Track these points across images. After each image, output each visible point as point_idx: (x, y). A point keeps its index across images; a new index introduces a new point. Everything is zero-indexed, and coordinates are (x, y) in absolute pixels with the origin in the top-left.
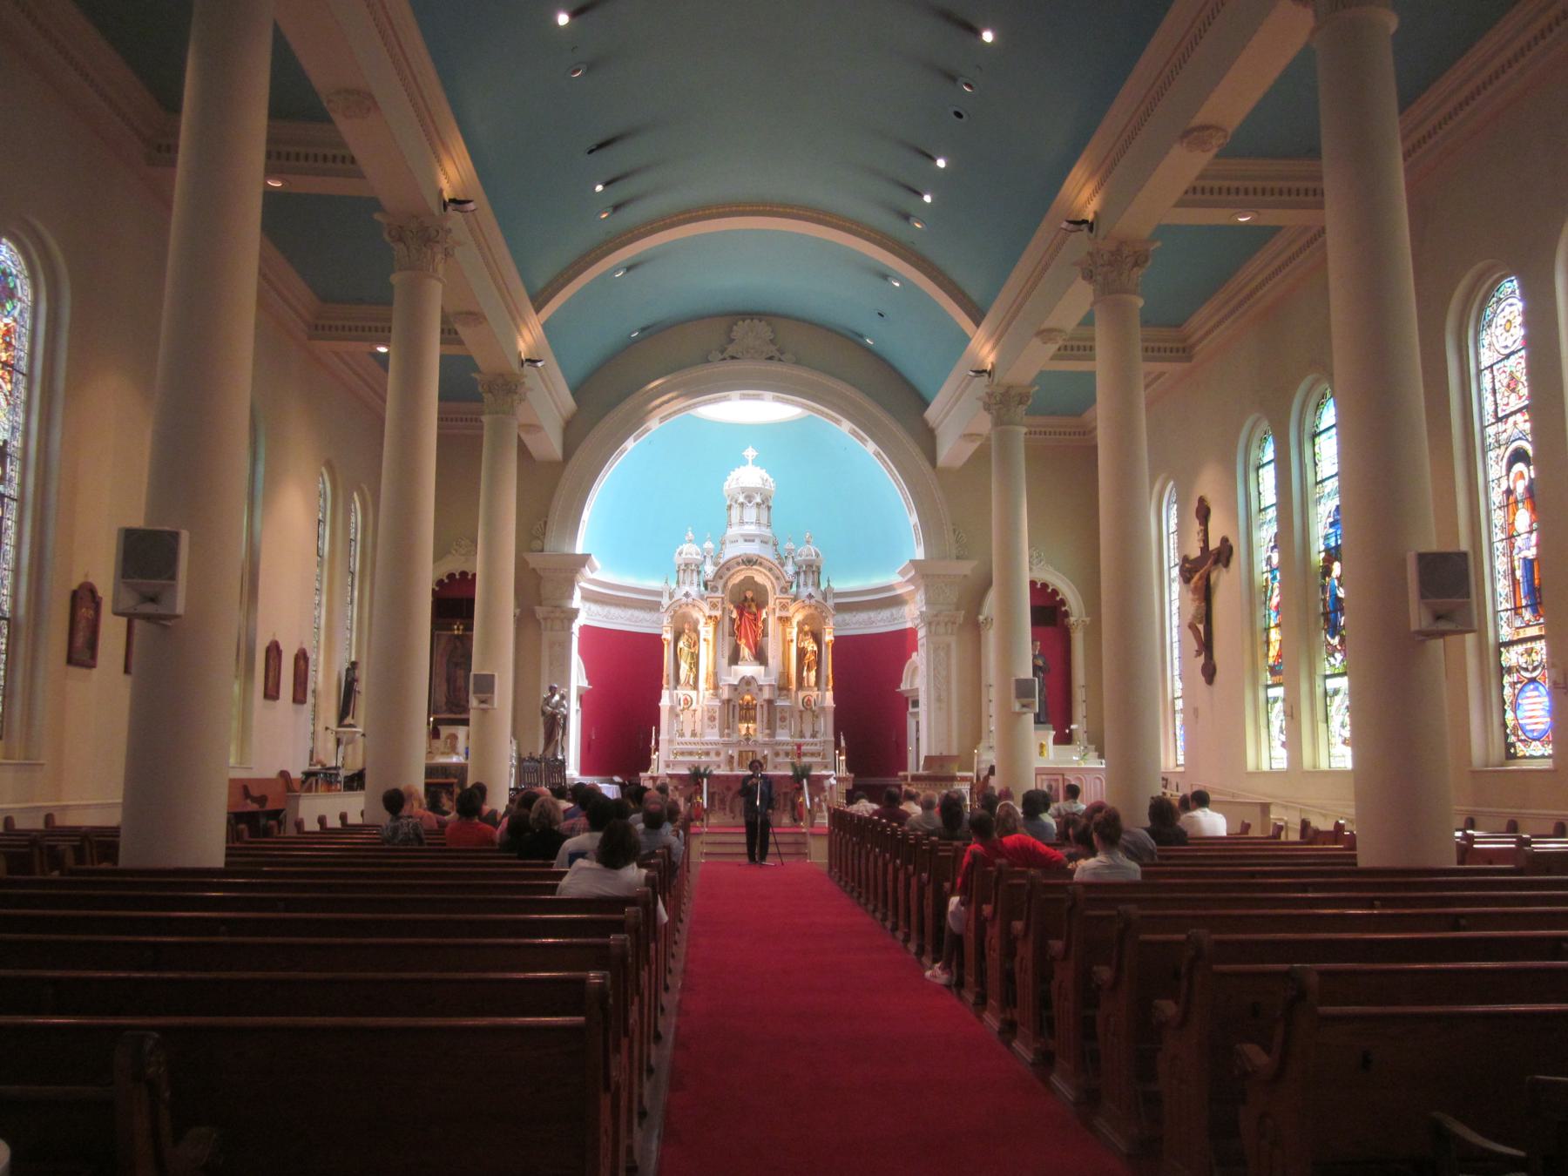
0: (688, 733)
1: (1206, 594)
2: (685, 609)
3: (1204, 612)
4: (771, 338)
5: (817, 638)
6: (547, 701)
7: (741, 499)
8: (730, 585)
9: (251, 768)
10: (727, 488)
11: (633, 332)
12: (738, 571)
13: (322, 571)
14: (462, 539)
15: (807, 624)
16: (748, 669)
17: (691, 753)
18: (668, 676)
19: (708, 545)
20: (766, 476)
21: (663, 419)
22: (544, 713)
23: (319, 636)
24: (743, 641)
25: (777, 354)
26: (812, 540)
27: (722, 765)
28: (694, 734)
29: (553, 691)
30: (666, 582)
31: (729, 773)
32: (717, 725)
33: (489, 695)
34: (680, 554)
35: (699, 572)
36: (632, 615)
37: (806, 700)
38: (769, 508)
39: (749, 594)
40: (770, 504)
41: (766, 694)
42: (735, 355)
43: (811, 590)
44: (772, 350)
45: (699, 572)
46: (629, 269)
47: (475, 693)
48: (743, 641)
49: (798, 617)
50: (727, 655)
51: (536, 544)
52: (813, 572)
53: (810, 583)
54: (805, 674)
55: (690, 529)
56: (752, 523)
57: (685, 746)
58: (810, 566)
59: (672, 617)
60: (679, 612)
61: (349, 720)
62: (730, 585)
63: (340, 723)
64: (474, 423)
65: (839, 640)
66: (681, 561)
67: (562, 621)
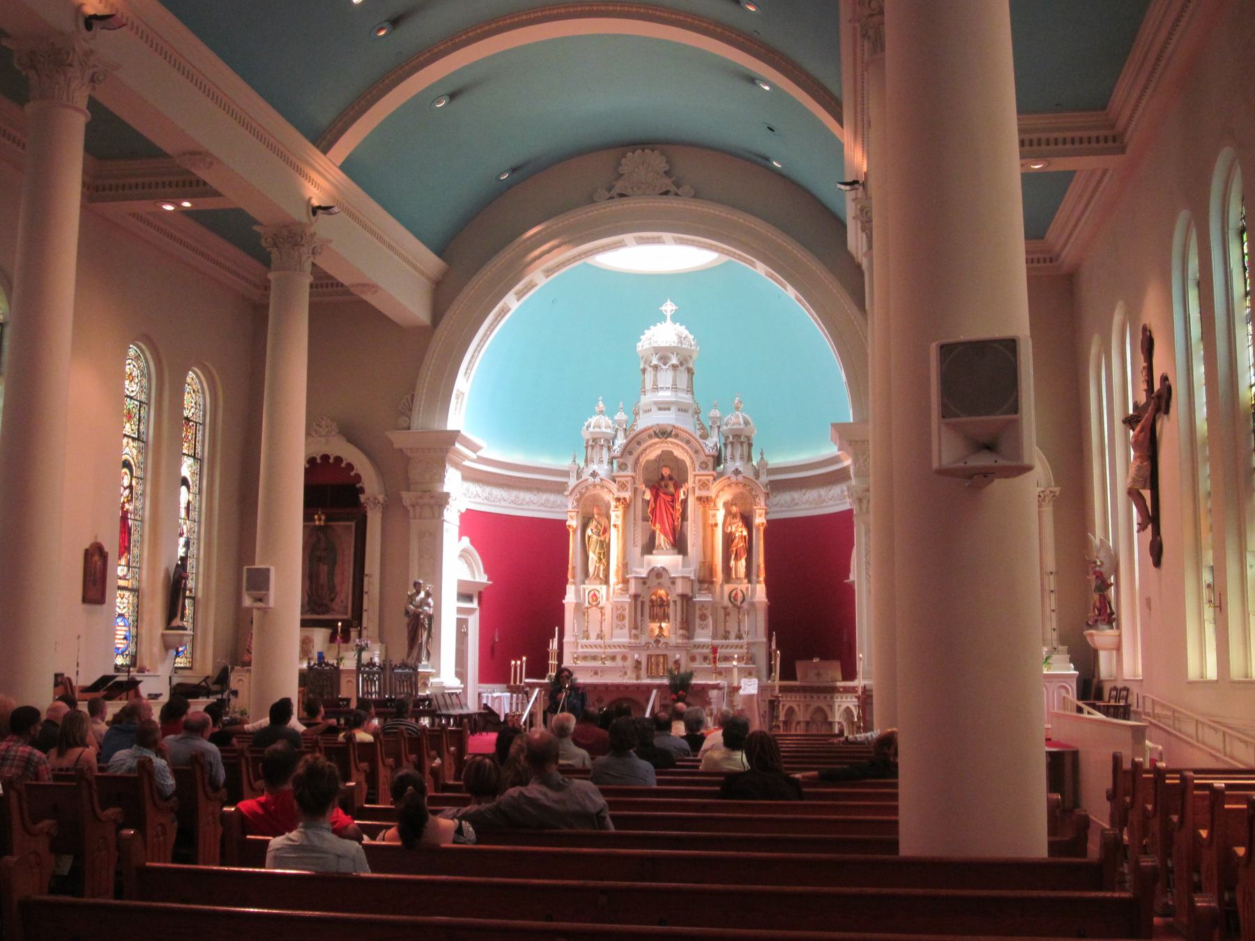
0: (593, 635)
1: (1149, 448)
2: (592, 492)
3: (1148, 474)
4: (666, 169)
5: (747, 521)
6: (411, 599)
7: (655, 362)
8: (643, 461)
9: (159, 676)
10: (640, 349)
11: (502, 174)
12: (651, 446)
13: (146, 458)
14: (322, 419)
15: (735, 505)
16: (665, 559)
17: (594, 658)
18: (574, 568)
19: (621, 416)
20: (685, 332)
21: (548, 272)
22: (407, 613)
23: (142, 528)
24: (658, 526)
25: (673, 188)
26: (742, 406)
27: (629, 673)
28: (600, 636)
29: (417, 586)
30: (574, 461)
31: (634, 682)
32: (627, 625)
33: (263, 592)
34: (588, 427)
35: (609, 449)
36: (517, 497)
37: (733, 595)
38: (690, 372)
39: (666, 472)
40: (691, 366)
41: (680, 588)
42: (624, 193)
43: (738, 464)
44: (667, 183)
45: (609, 449)
46: (452, 96)
47: (248, 589)
48: (658, 526)
49: (726, 496)
50: (640, 544)
51: (402, 421)
52: (742, 443)
53: (738, 456)
54: (732, 563)
55: (601, 398)
56: (668, 388)
57: (590, 650)
58: (737, 436)
59: (578, 501)
60: (586, 495)
61: (176, 622)
62: (643, 461)
63: (168, 626)
64: (325, 289)
65: (774, 528)
66: (588, 437)
67: (432, 507)
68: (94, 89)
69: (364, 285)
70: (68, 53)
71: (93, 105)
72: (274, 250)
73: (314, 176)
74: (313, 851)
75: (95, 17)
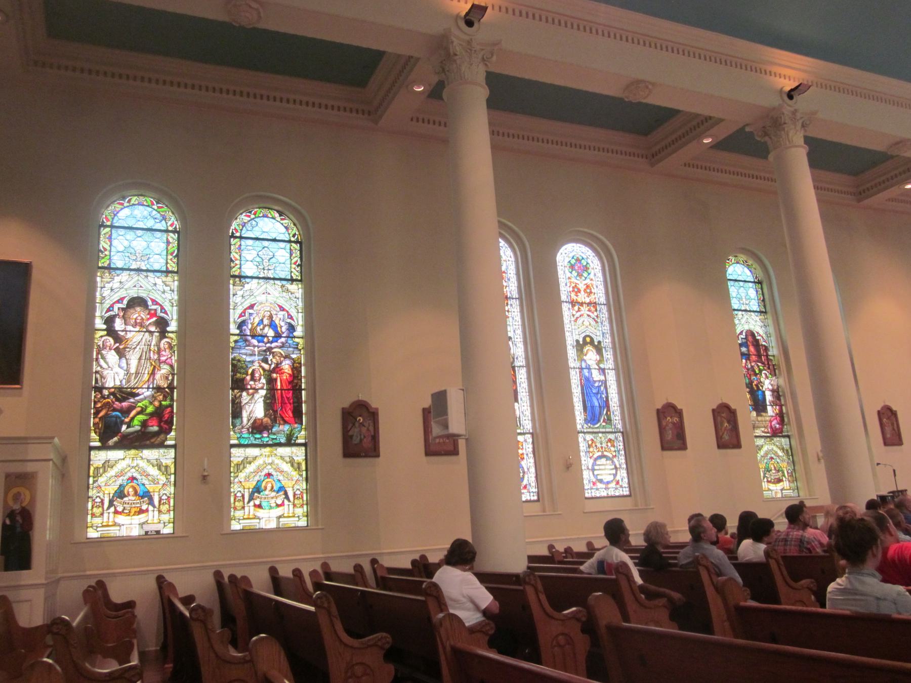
68: (805, 131)
69: (897, 143)
70: (781, 117)
71: (808, 140)
72: (767, 138)
73: (775, 69)
74: (856, 594)
75: (792, 90)
